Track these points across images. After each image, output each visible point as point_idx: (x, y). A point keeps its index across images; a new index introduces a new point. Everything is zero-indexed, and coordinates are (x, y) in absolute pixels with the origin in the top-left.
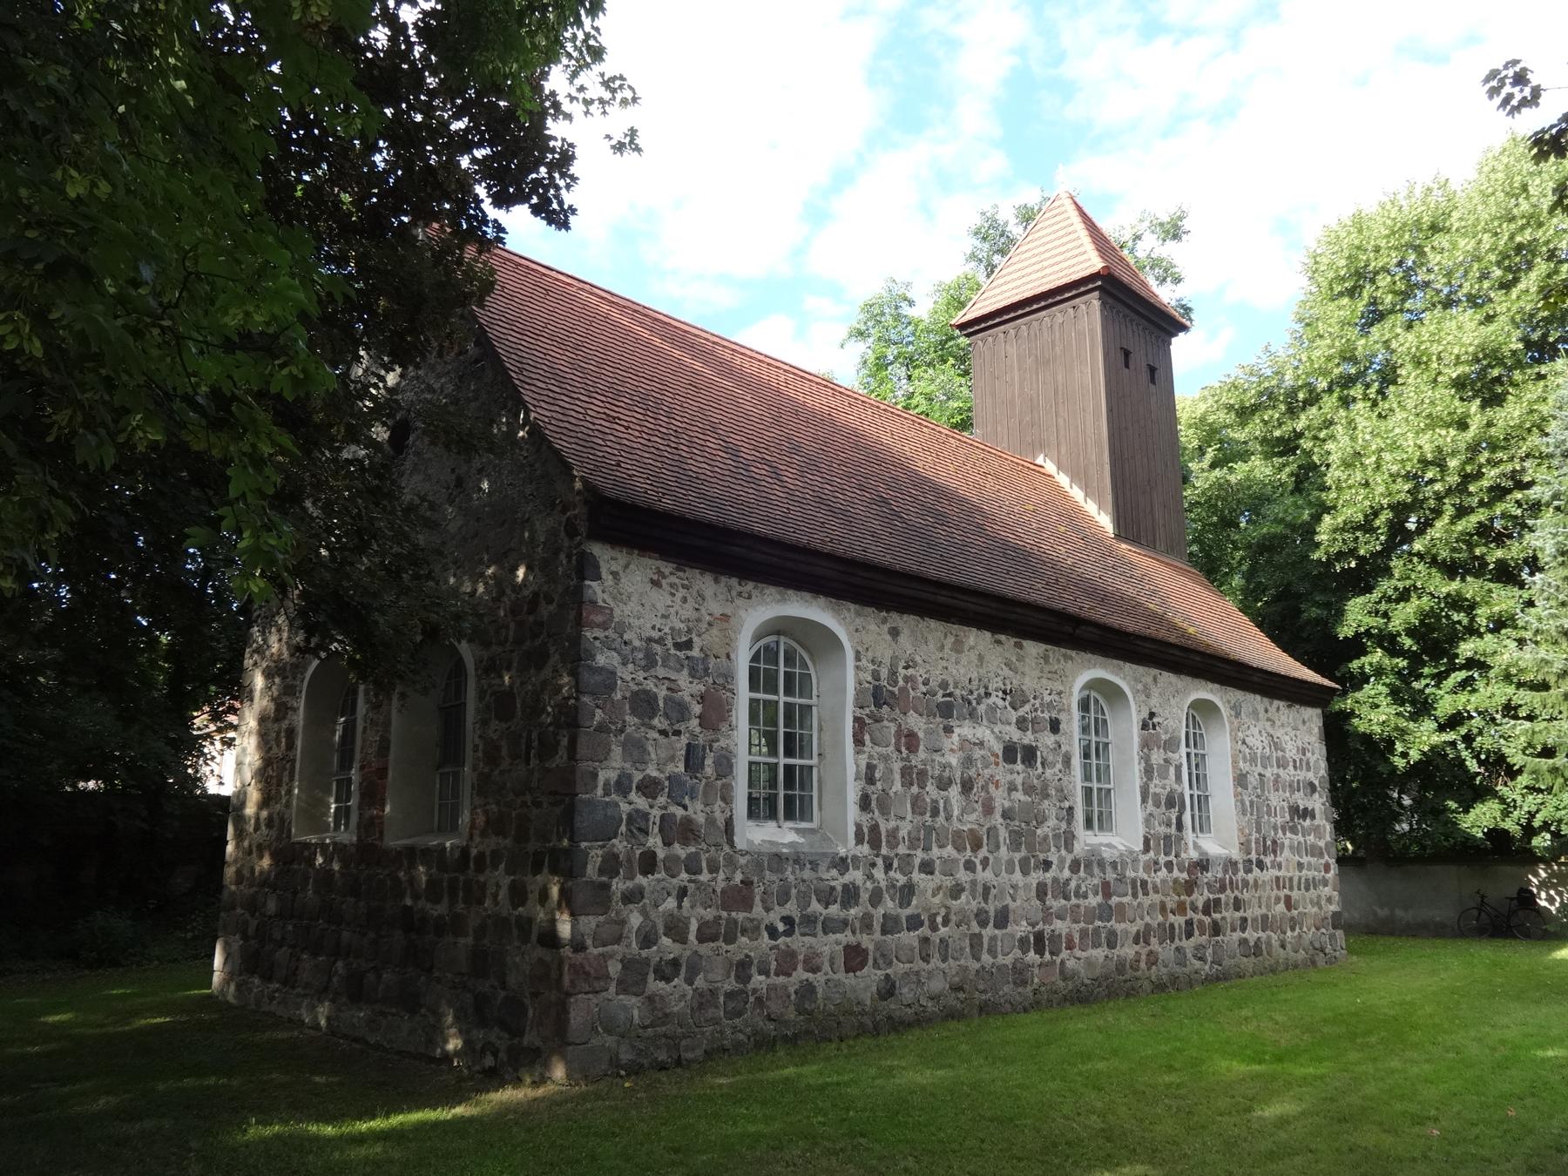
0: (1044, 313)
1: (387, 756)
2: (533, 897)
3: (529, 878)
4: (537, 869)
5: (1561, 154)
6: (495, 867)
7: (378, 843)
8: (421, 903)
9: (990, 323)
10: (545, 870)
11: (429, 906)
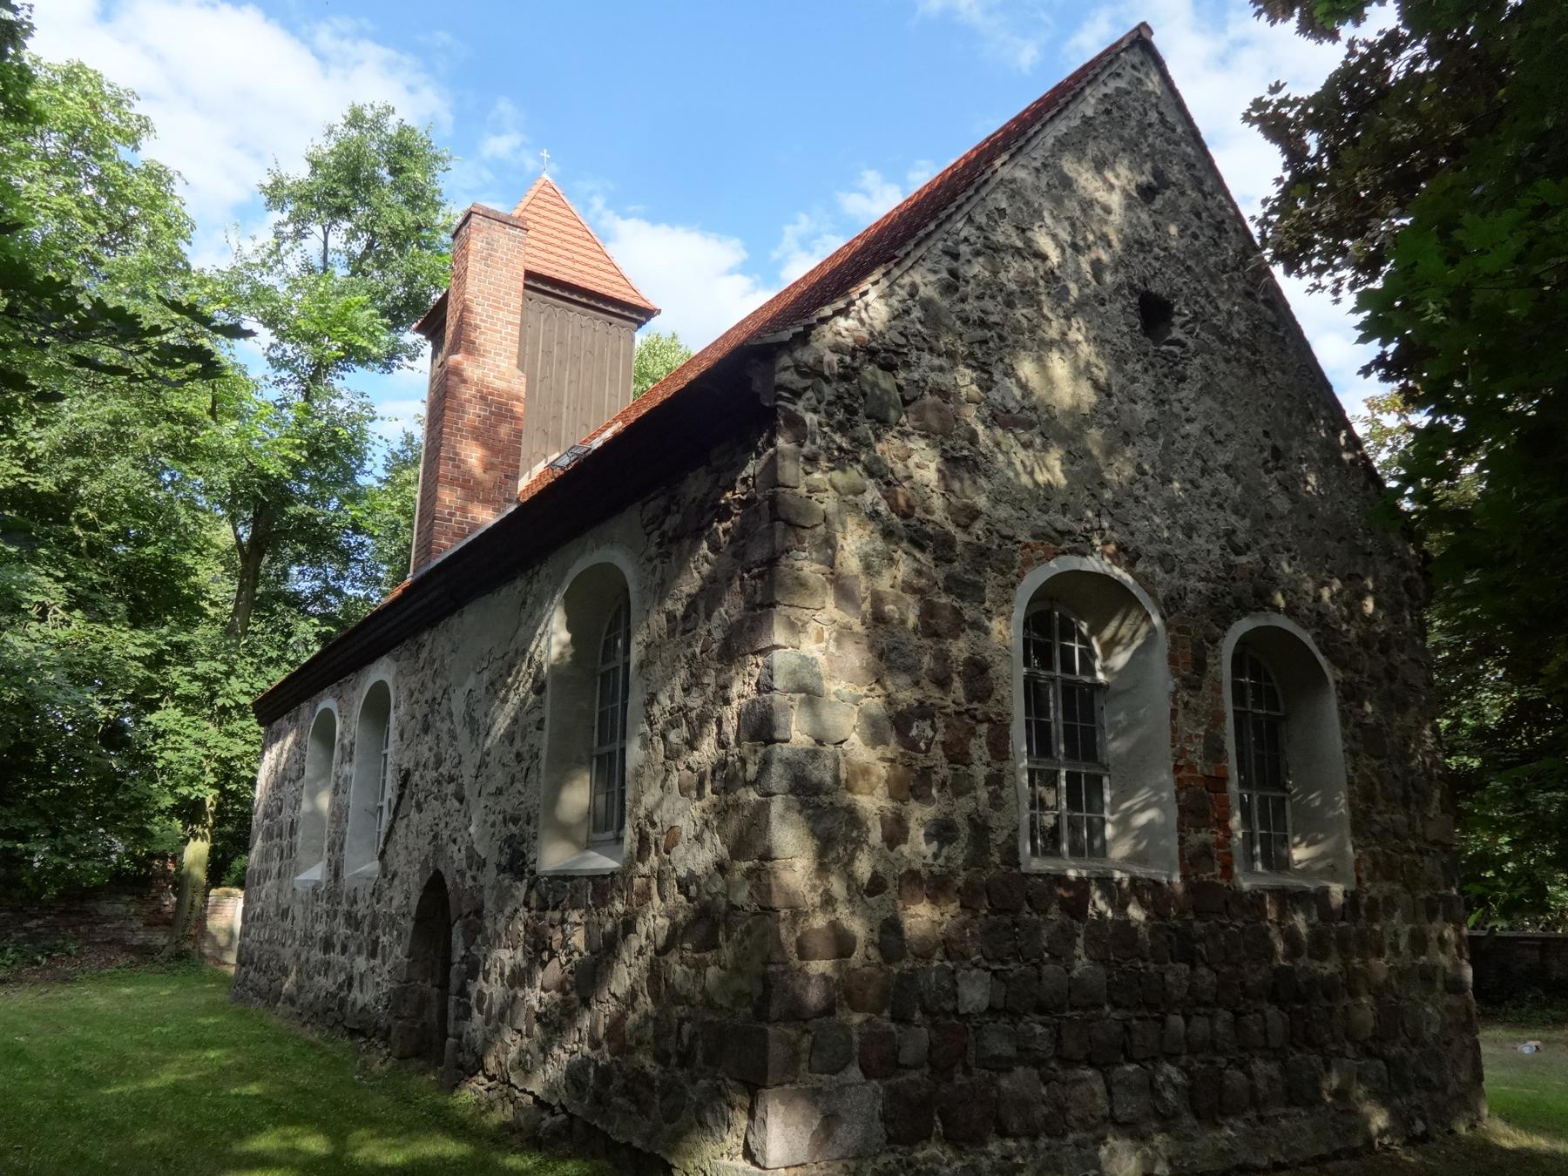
0: (579, 309)
1: (1224, 790)
2: (1433, 945)
3: (1427, 926)
4: (1432, 915)
5: (20, 497)
6: (1389, 916)
7: (1224, 882)
8: (1303, 961)
9: (557, 292)
10: (1440, 918)
11: (1316, 964)
